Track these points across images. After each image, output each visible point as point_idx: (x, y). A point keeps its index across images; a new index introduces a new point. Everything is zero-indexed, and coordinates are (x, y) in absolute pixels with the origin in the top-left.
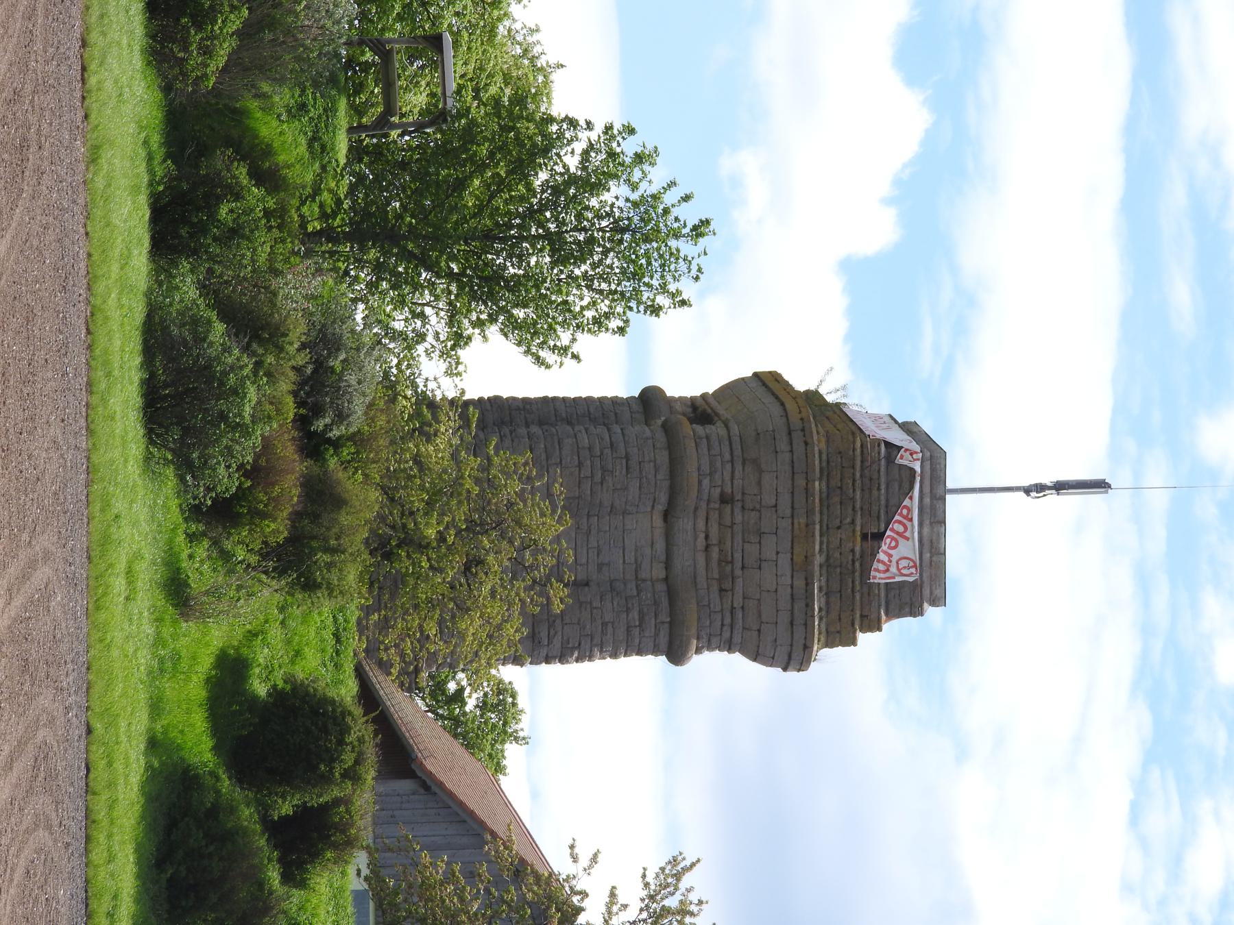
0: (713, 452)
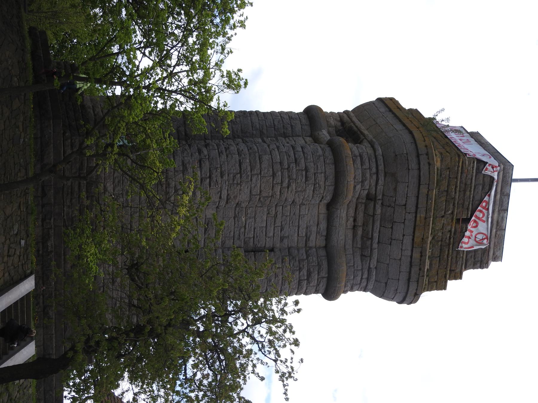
0: (364, 167)
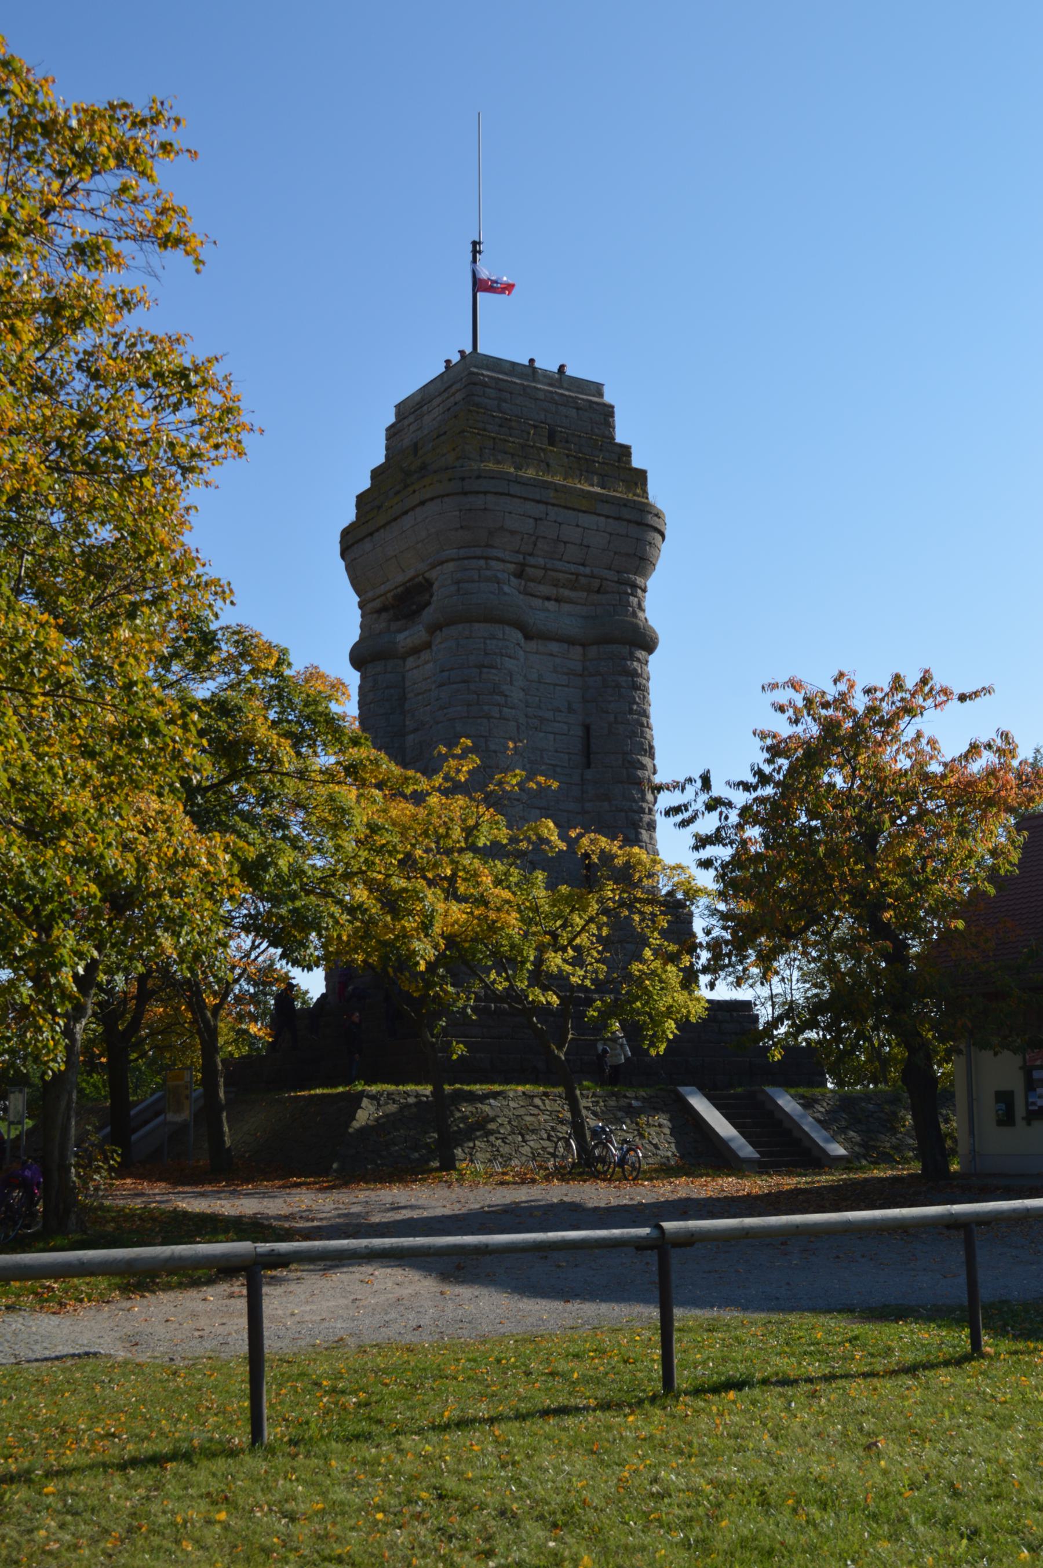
0: (476, 577)
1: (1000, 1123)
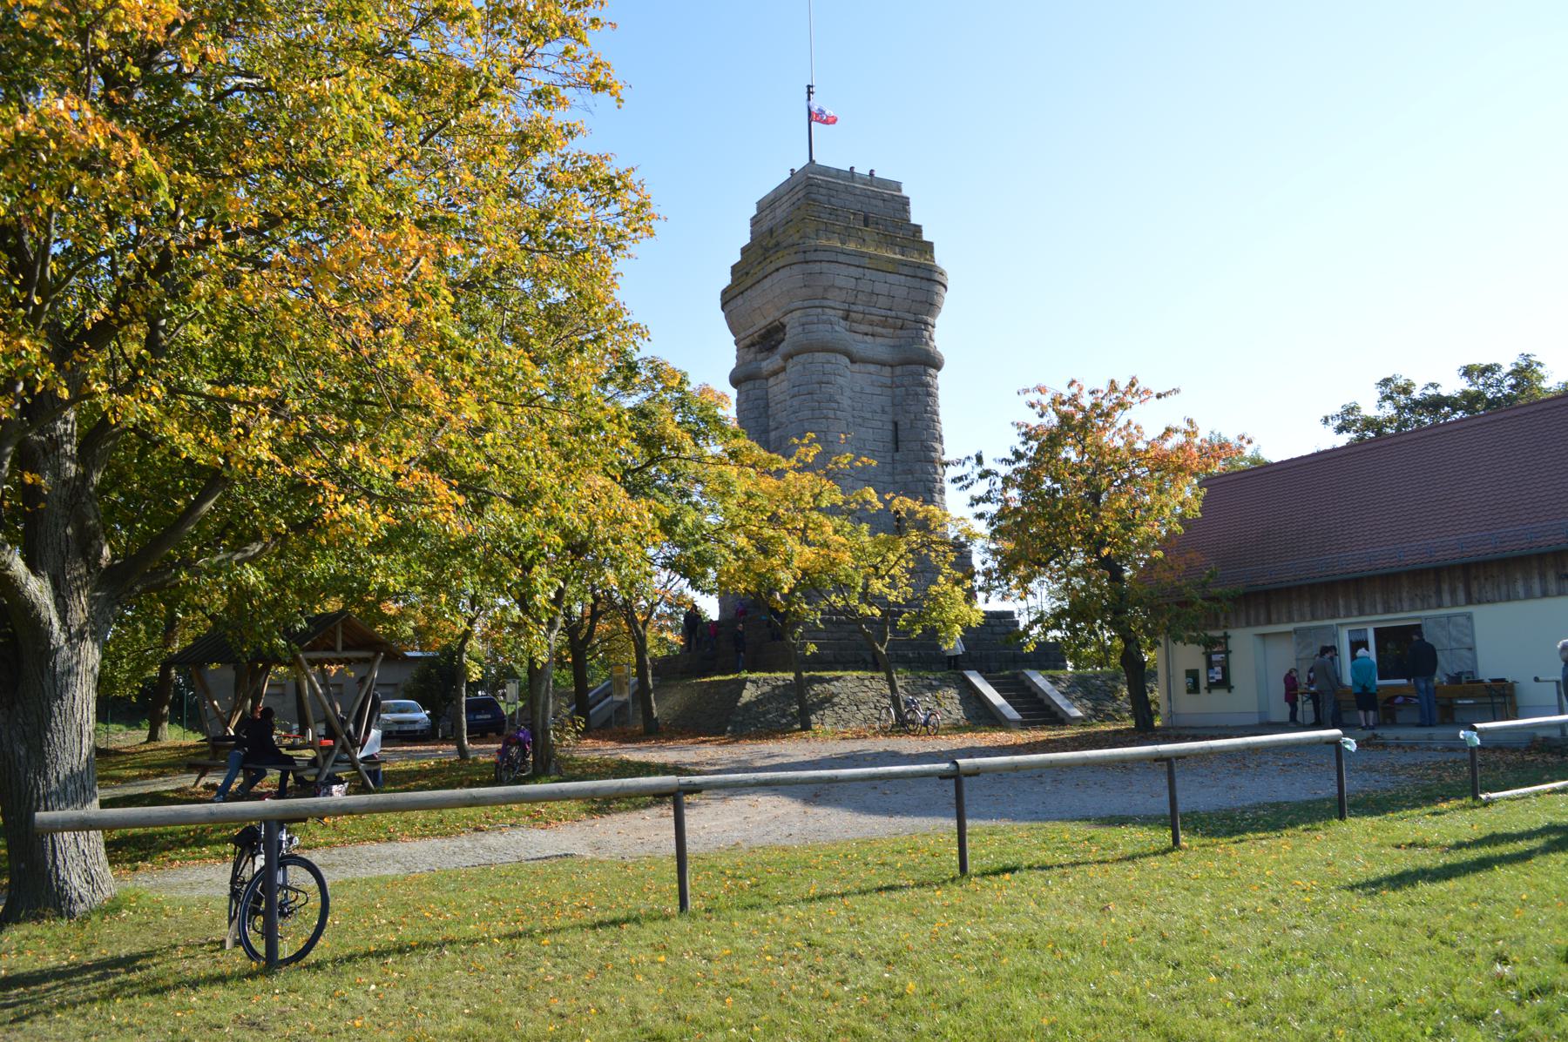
1: (1189, 692)
